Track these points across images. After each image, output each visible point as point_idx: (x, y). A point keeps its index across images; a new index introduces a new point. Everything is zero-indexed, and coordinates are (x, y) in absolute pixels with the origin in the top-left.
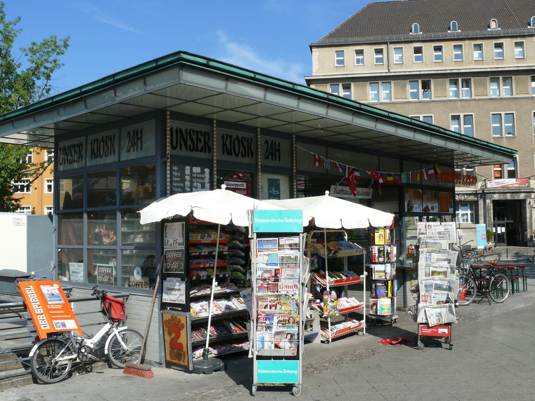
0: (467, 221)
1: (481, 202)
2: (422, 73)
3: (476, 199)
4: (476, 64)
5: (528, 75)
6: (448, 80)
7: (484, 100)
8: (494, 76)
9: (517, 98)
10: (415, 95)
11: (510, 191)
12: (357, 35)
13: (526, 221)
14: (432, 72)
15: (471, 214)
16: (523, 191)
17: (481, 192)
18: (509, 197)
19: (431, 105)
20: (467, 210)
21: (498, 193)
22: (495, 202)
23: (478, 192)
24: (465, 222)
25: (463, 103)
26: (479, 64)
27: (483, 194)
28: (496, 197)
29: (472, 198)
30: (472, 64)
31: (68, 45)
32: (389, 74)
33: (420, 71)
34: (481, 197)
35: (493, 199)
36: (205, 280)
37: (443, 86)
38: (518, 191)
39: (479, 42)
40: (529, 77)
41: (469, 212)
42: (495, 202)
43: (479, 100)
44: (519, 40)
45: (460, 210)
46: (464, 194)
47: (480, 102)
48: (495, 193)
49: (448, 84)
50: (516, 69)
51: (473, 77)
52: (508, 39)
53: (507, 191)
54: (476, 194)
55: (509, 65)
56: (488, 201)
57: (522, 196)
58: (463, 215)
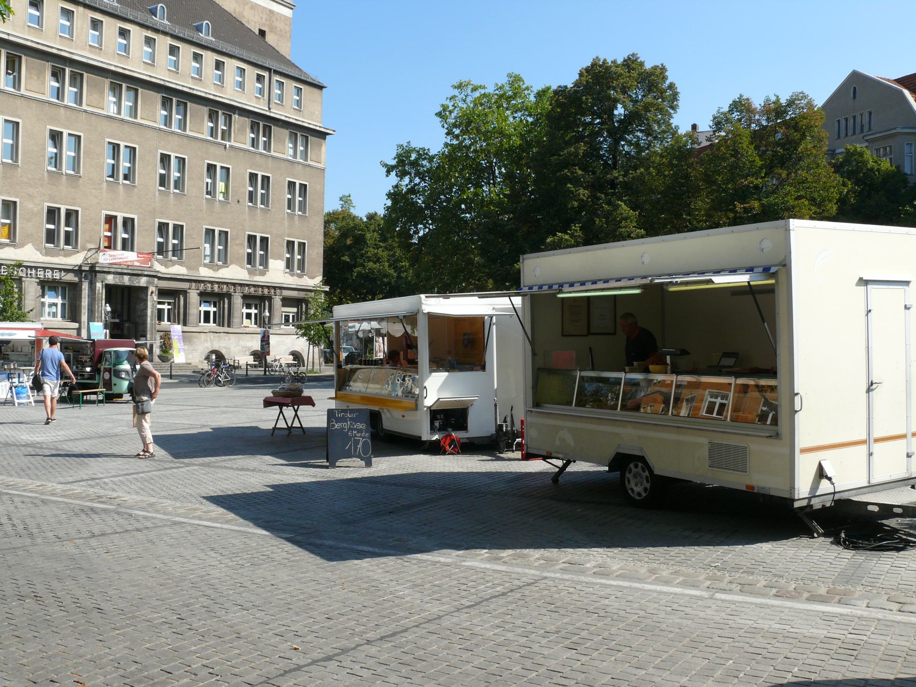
0: (55, 315)
1: (85, 286)
2: (12, 38)
3: (76, 279)
4: (90, 52)
5: (159, 92)
6: (107, 82)
7: (99, 115)
8: (120, 81)
9: (141, 125)
10: (254, 143)
11: (129, 271)
12: (242, 46)
13: (146, 320)
14: (29, 44)
15: (63, 305)
16: (146, 273)
17: (87, 269)
18: (126, 281)
19: (19, 102)
20: (57, 297)
21: (114, 273)
22: (109, 288)
23: (83, 268)
24: (51, 318)
25: (69, 113)
26: (95, 54)
27: (91, 272)
28: (111, 279)
29: (70, 277)
30: (85, 50)
31: (439, 114)
32: (268, 114)
33: (8, 34)
34: (86, 278)
35: (107, 282)
36: (381, 360)
37: (40, 74)
38: (140, 272)
39: (98, 16)
40: (107, 82)
41: (59, 301)
42: (109, 288)
43: (93, 113)
44: (150, 34)
45: (46, 297)
46: (60, 270)
47: (93, 118)
48: (109, 273)
49: (48, 73)
50: (148, 79)
51: (25, 55)
52: (137, 28)
53: (126, 271)
54: (78, 271)
55: (136, 67)
56: (99, 285)
57: (143, 282)
58: (51, 305)
